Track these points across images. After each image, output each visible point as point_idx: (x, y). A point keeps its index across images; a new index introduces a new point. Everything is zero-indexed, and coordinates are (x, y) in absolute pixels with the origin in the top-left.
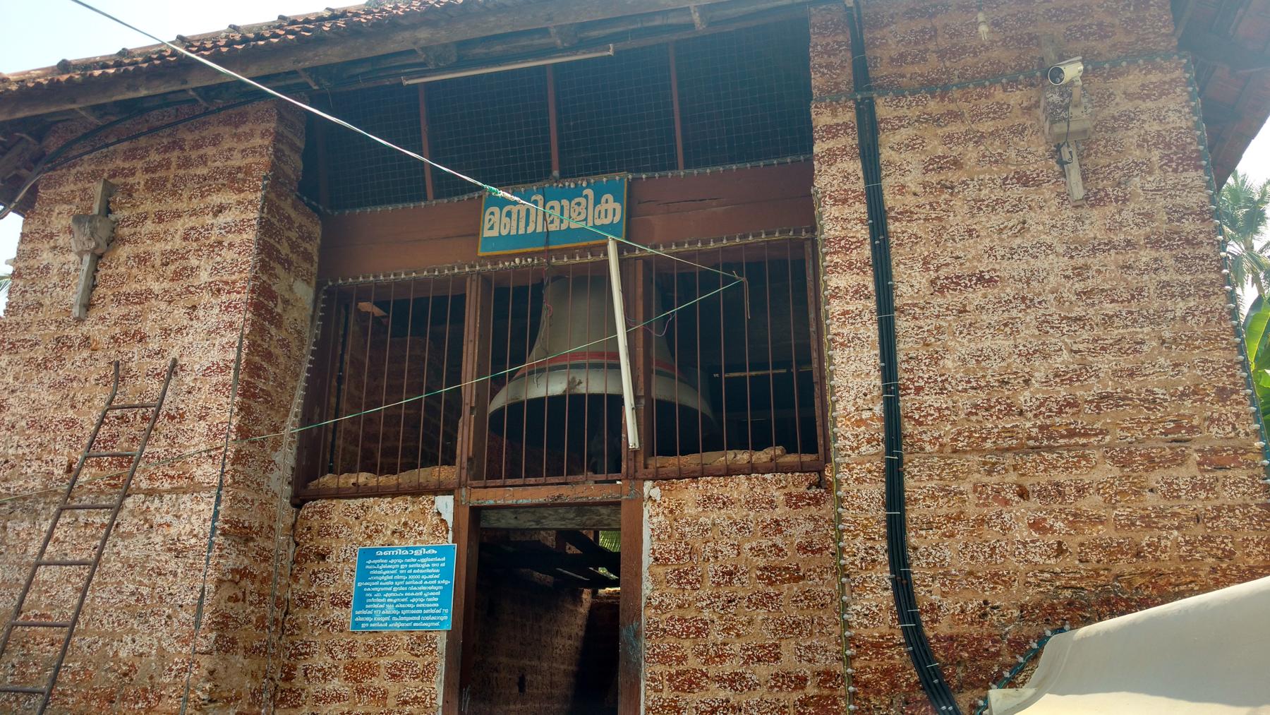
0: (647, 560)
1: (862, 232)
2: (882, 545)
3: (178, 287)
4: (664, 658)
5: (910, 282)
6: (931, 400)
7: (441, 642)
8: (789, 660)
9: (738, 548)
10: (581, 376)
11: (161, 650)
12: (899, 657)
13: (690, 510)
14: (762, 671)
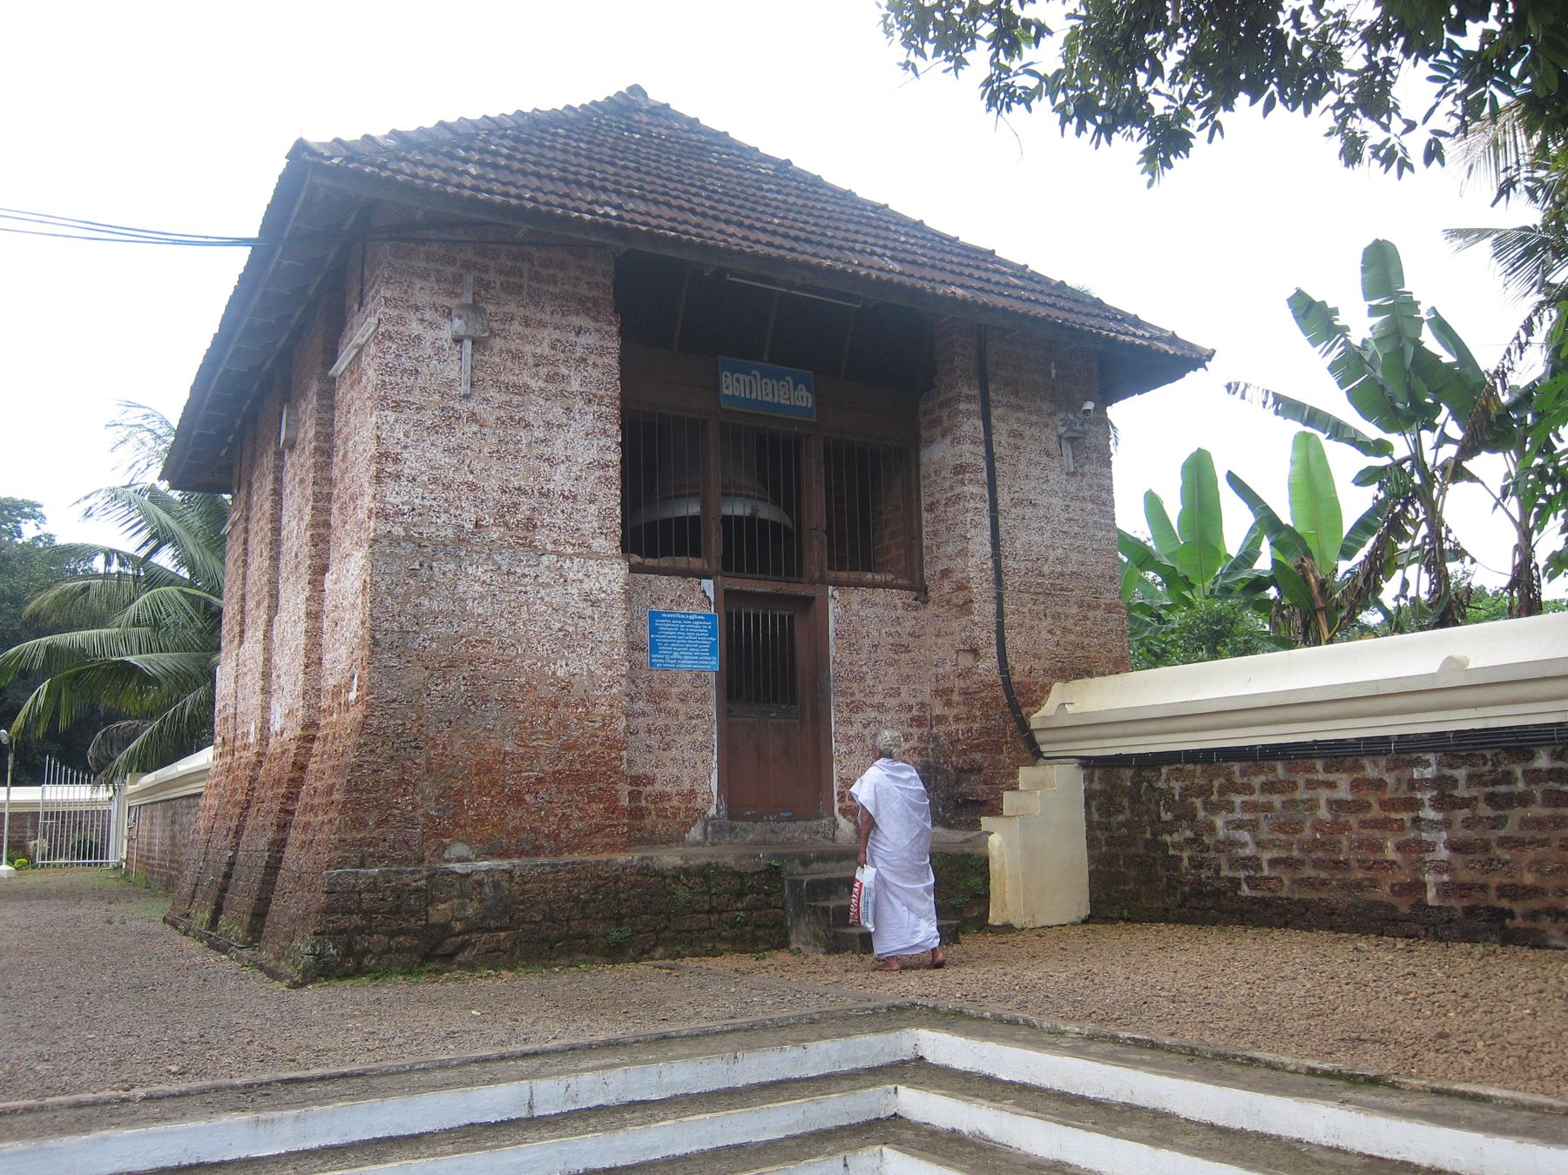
0: (832, 635)
1: (983, 464)
2: (994, 636)
3: (552, 388)
4: (843, 693)
5: (1004, 499)
6: (1010, 562)
7: (712, 678)
8: (905, 696)
9: (879, 631)
10: (760, 505)
11: (589, 671)
12: (1000, 692)
13: (855, 607)
14: (891, 702)
